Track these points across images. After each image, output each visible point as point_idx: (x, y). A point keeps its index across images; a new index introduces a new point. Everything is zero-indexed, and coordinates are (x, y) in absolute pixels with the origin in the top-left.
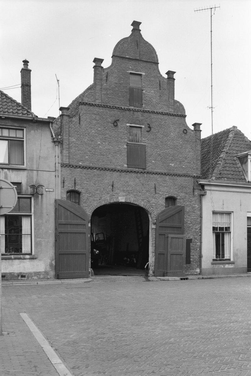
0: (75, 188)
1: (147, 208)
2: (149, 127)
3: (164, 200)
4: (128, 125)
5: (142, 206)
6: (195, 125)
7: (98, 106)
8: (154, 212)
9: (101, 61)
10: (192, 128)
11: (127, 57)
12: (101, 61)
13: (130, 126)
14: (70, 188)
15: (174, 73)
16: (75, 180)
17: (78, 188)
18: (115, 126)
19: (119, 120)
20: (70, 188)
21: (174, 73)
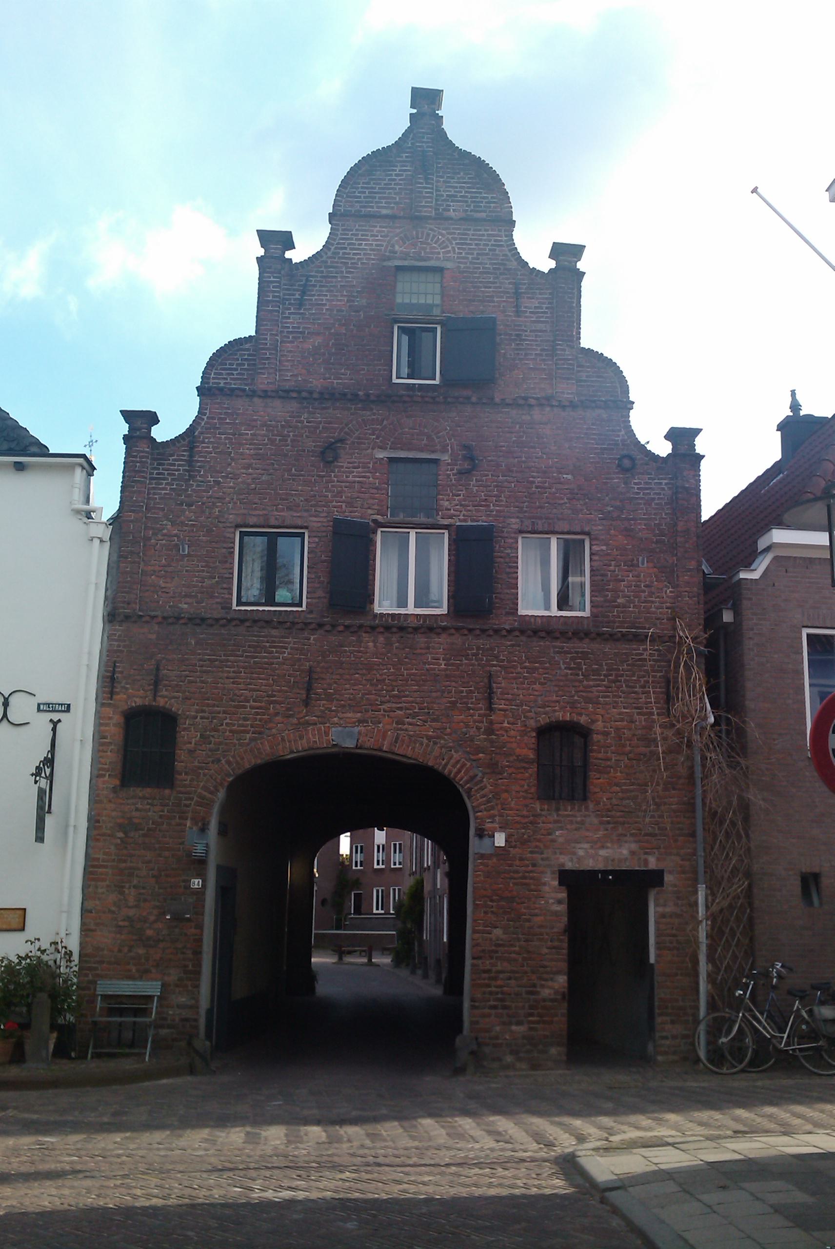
0: (155, 700)
1: (450, 772)
2: (472, 459)
3: (531, 739)
4: (381, 454)
5: (430, 764)
6: (559, 251)
7: (265, 395)
8: (482, 789)
9: (152, 418)
10: (663, 449)
11: (384, 212)
12: (152, 418)
13: (391, 460)
14: (137, 700)
15: (697, 431)
16: (158, 669)
17: (165, 700)
18: (328, 462)
19: (342, 441)
20: (137, 700)
21: (577, 251)
